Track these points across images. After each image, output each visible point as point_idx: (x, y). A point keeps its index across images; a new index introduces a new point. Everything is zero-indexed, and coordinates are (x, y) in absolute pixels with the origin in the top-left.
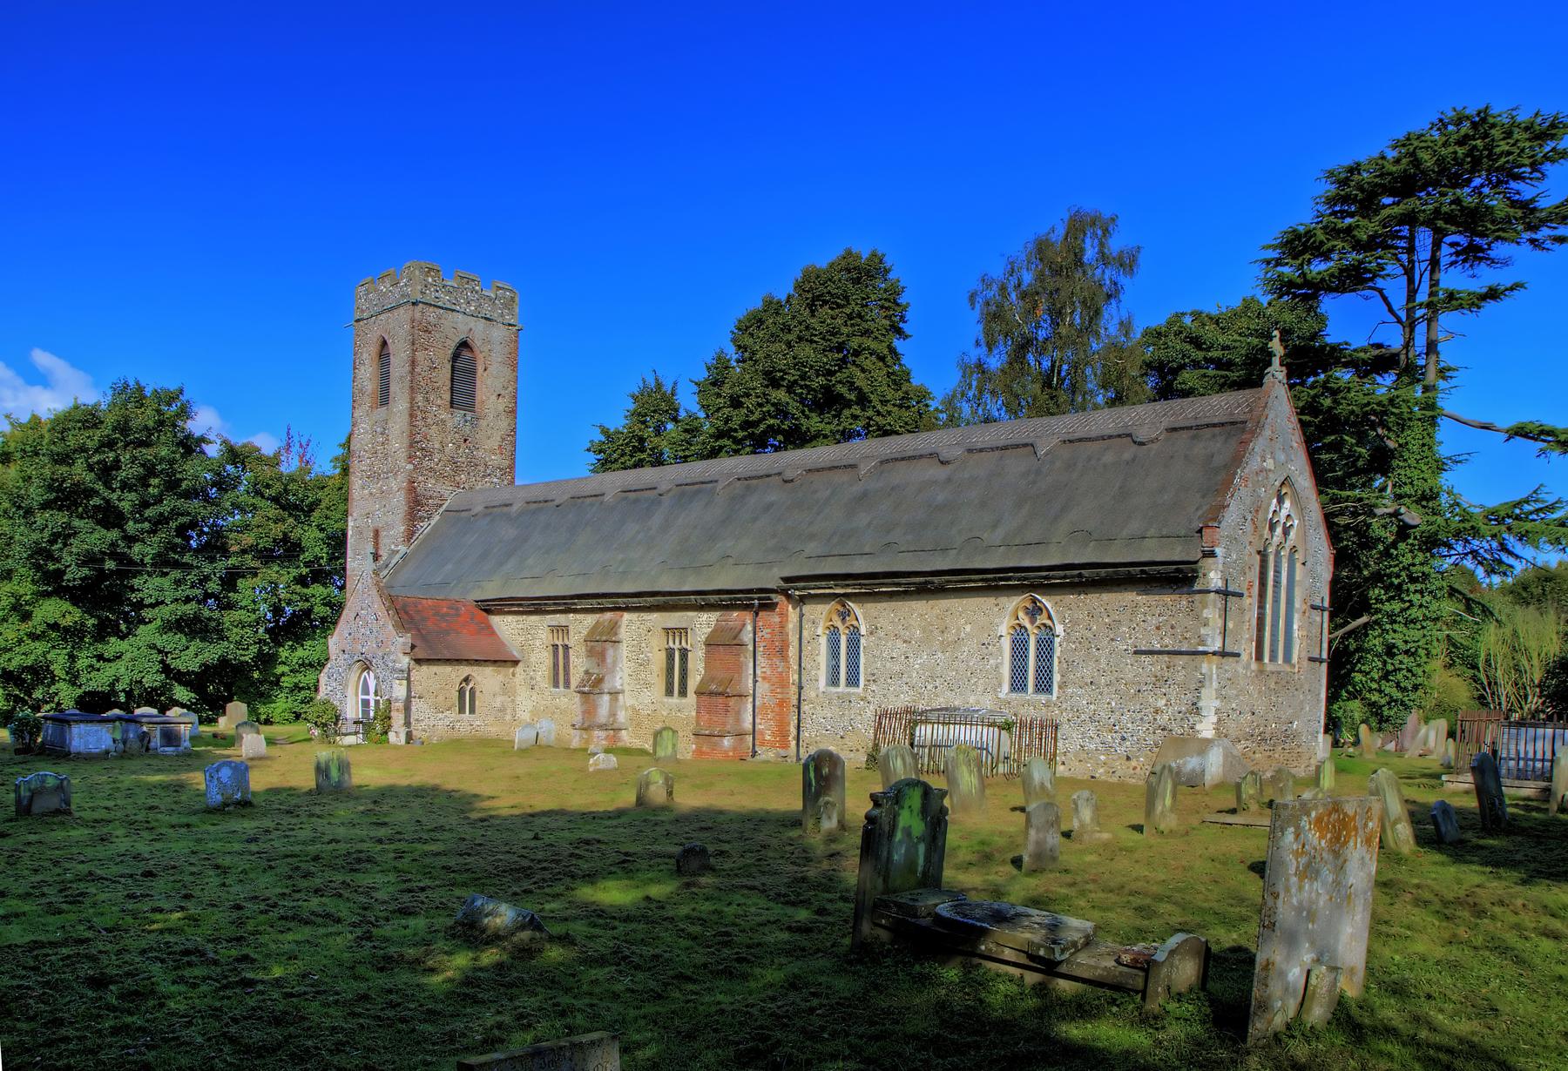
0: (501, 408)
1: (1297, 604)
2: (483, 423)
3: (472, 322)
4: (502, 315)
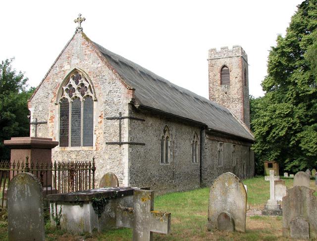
0: (237, 81)
1: (96, 119)
2: (231, 87)
3: (226, 60)
4: (236, 55)
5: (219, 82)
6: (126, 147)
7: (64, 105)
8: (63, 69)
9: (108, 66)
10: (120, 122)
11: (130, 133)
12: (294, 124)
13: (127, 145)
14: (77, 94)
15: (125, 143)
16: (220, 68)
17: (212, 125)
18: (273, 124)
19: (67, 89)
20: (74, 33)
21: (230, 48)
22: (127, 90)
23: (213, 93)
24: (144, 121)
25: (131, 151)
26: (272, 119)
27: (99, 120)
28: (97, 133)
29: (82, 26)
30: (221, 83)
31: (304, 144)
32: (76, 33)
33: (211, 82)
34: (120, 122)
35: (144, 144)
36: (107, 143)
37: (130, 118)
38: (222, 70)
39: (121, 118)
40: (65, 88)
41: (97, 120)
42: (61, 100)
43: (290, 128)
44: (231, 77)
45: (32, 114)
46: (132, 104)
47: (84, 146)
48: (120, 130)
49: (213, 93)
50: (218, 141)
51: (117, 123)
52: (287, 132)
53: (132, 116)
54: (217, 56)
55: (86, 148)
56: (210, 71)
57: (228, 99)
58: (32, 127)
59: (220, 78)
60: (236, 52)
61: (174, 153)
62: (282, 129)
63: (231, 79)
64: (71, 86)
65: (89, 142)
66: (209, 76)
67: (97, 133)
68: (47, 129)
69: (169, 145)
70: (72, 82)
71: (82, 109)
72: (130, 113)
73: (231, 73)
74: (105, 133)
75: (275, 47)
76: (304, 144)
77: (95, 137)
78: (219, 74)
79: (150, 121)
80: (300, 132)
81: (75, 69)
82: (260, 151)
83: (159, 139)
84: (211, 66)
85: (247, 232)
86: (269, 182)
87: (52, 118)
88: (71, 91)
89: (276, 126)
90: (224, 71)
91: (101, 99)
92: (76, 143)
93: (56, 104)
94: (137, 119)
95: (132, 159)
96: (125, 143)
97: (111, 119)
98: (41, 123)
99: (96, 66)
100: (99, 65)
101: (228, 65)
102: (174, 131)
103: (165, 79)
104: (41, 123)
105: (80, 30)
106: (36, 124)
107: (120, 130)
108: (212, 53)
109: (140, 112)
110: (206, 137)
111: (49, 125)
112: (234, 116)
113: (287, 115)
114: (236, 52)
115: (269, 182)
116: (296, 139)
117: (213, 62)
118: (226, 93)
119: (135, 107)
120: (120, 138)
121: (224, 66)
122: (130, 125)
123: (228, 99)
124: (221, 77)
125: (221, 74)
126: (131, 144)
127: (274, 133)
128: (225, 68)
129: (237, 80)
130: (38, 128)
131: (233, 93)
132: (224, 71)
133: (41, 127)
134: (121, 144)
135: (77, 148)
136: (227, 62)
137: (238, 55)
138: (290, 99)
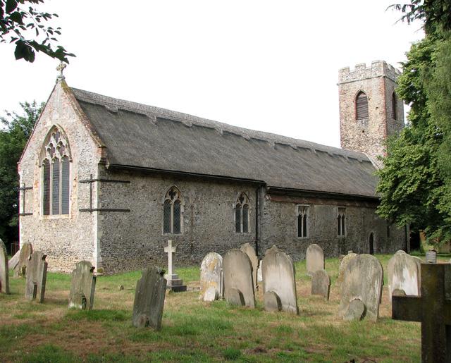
1: (72, 183)
3: (362, 83)
4: (376, 74)
5: (354, 116)
6: (95, 213)
7: (46, 165)
8: (46, 126)
9: (82, 120)
10: (91, 185)
11: (100, 198)
12: (429, 175)
13: (96, 212)
14: (57, 153)
15: (95, 210)
16: (354, 95)
17: (273, 181)
18: (399, 176)
19: (49, 149)
20: (55, 84)
21: (369, 65)
22: (97, 148)
23: (346, 132)
24: (129, 182)
25: (103, 219)
26: (399, 169)
27: (74, 183)
28: (72, 198)
29: (63, 74)
30: (357, 118)
31: (444, 205)
32: (57, 83)
33: (343, 116)
34: (91, 185)
35: (129, 211)
36: (80, 210)
37: (101, 180)
38: (357, 98)
39: (91, 181)
40: (47, 147)
41: (72, 183)
42: (44, 161)
43: (423, 182)
44: (369, 108)
45: (21, 179)
46: (102, 163)
47: (63, 214)
48: (91, 195)
49: (346, 132)
50: (297, 204)
51: (88, 186)
52: (419, 187)
53: (105, 178)
54: (350, 78)
55: (64, 216)
56: (341, 100)
57: (366, 141)
58: (21, 193)
59: (354, 111)
60: (377, 70)
61: (192, 221)
62: (413, 183)
63: (369, 111)
64: (51, 145)
65: (66, 211)
66: (340, 108)
67: (72, 198)
68: (33, 195)
69: (182, 210)
70: (53, 140)
71: (61, 171)
72: (101, 173)
73: (369, 102)
74: (79, 198)
75: (405, 63)
76: (444, 205)
77: (70, 202)
78: (354, 104)
79: (140, 183)
80: (437, 186)
81: (54, 126)
82: (387, 215)
83: (158, 204)
84: (343, 93)
85: (10, 294)
86: (167, 253)
87: (37, 182)
88: (51, 151)
89: (403, 178)
90: (360, 100)
91: (76, 159)
92: (56, 212)
93: (40, 167)
94: (117, 182)
95: (103, 227)
96: (95, 210)
97: (84, 182)
98: (28, 189)
99: (72, 121)
100: (75, 120)
101: (365, 90)
102: (193, 192)
103: (231, 124)
104: (28, 189)
105: (60, 79)
106: (24, 189)
107: (91, 195)
108: (344, 74)
109: (115, 172)
110: (266, 200)
111: (35, 190)
112: (374, 165)
113: (419, 163)
114: (377, 70)
115: (167, 253)
116: (433, 198)
117: (345, 87)
118: (363, 132)
119: (106, 168)
120: (91, 204)
121: (361, 92)
122: (101, 188)
123: (366, 141)
124: (357, 108)
125: (357, 104)
126: (102, 211)
127: (401, 189)
128: (362, 96)
129: (378, 112)
130: (26, 193)
131: (373, 130)
132: (360, 100)
133: (28, 192)
134: (91, 211)
135: (57, 217)
136: (364, 86)
137: (378, 74)
138: (429, 138)
